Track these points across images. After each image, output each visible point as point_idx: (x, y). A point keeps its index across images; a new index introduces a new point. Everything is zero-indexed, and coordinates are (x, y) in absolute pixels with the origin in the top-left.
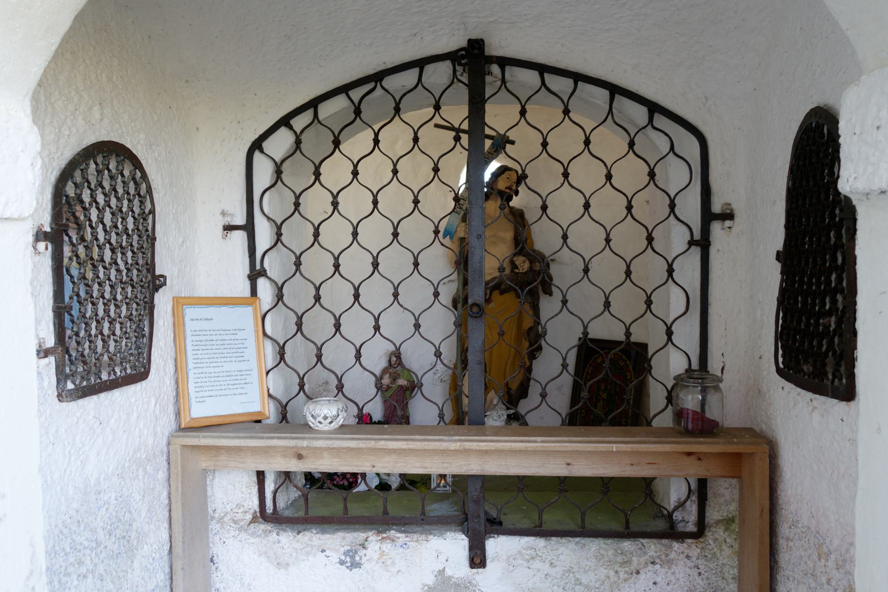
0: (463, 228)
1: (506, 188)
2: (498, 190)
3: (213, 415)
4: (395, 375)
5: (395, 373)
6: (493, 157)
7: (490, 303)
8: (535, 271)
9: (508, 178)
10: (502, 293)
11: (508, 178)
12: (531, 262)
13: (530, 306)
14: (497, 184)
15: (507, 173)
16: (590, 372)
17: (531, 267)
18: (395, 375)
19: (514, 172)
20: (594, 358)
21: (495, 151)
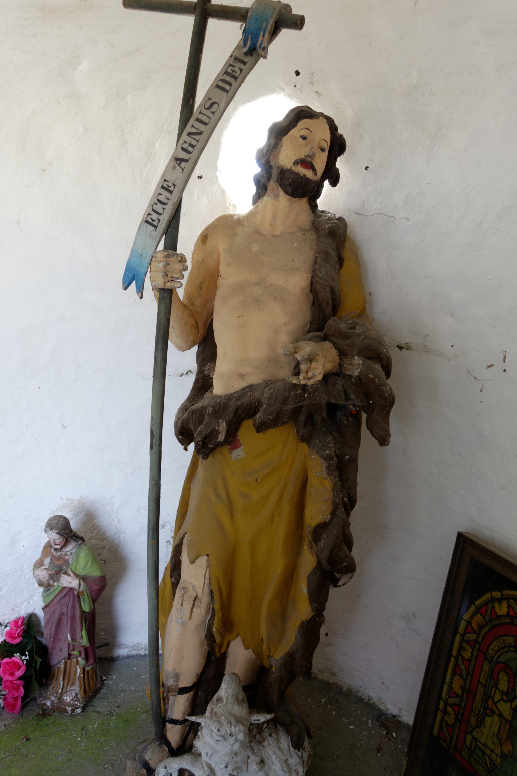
0: (161, 265)
1: (296, 163)
2: (278, 167)
3: (165, 390)
4: (60, 562)
5: (60, 558)
6: (245, 68)
7: (235, 448)
8: (350, 376)
9: (304, 138)
10: (260, 428)
11: (304, 138)
12: (342, 354)
13: (329, 468)
14: (279, 153)
15: (303, 123)
16: (474, 624)
17: (341, 366)
18: (60, 562)
19: (322, 120)
20: (488, 596)
21: (247, 54)
